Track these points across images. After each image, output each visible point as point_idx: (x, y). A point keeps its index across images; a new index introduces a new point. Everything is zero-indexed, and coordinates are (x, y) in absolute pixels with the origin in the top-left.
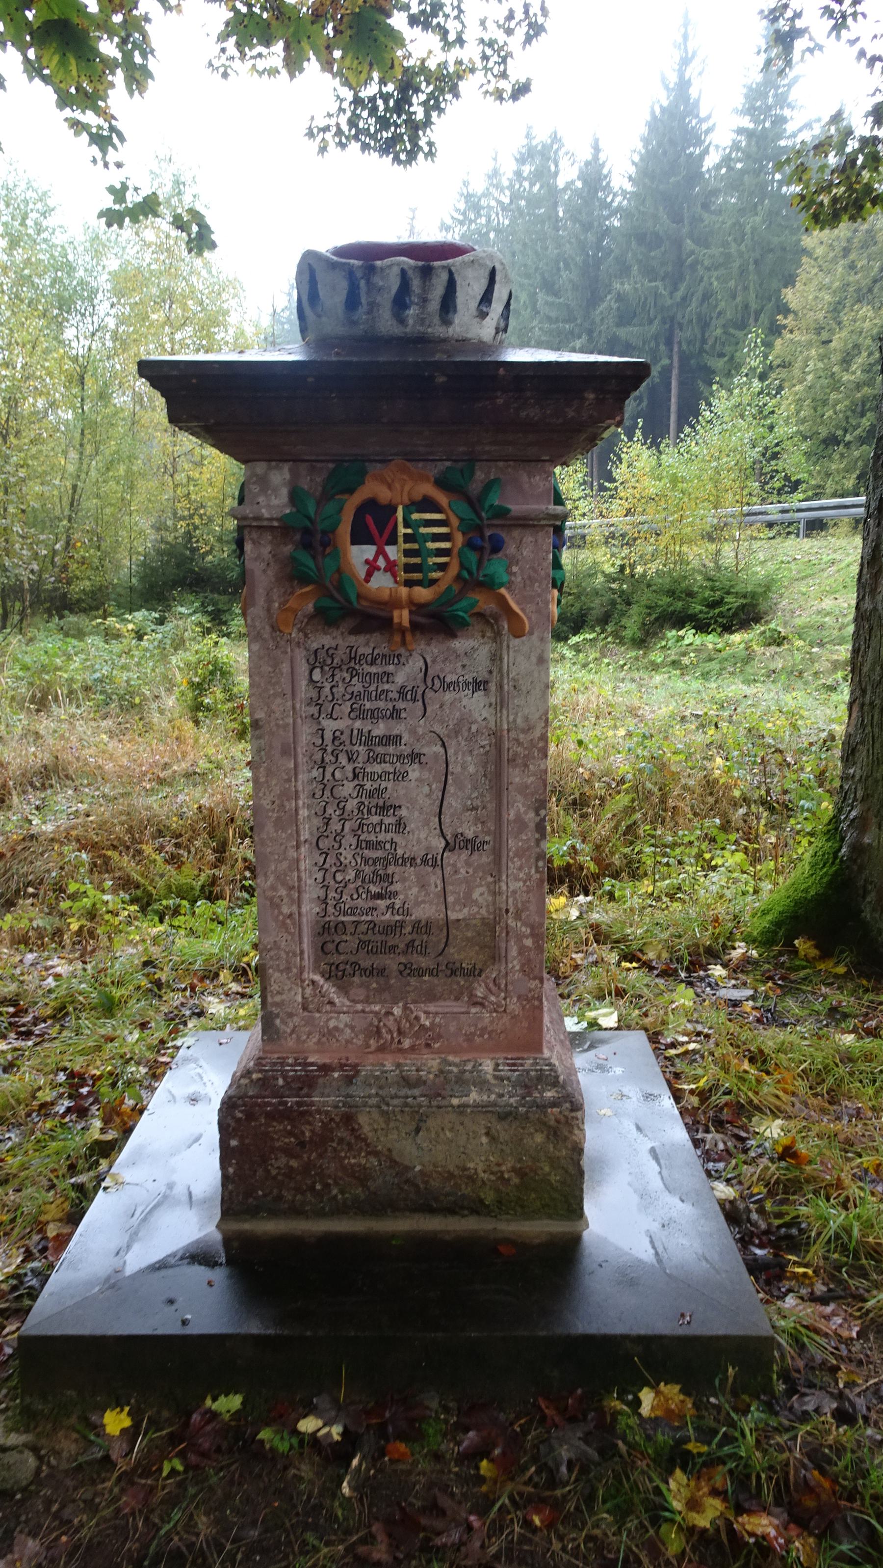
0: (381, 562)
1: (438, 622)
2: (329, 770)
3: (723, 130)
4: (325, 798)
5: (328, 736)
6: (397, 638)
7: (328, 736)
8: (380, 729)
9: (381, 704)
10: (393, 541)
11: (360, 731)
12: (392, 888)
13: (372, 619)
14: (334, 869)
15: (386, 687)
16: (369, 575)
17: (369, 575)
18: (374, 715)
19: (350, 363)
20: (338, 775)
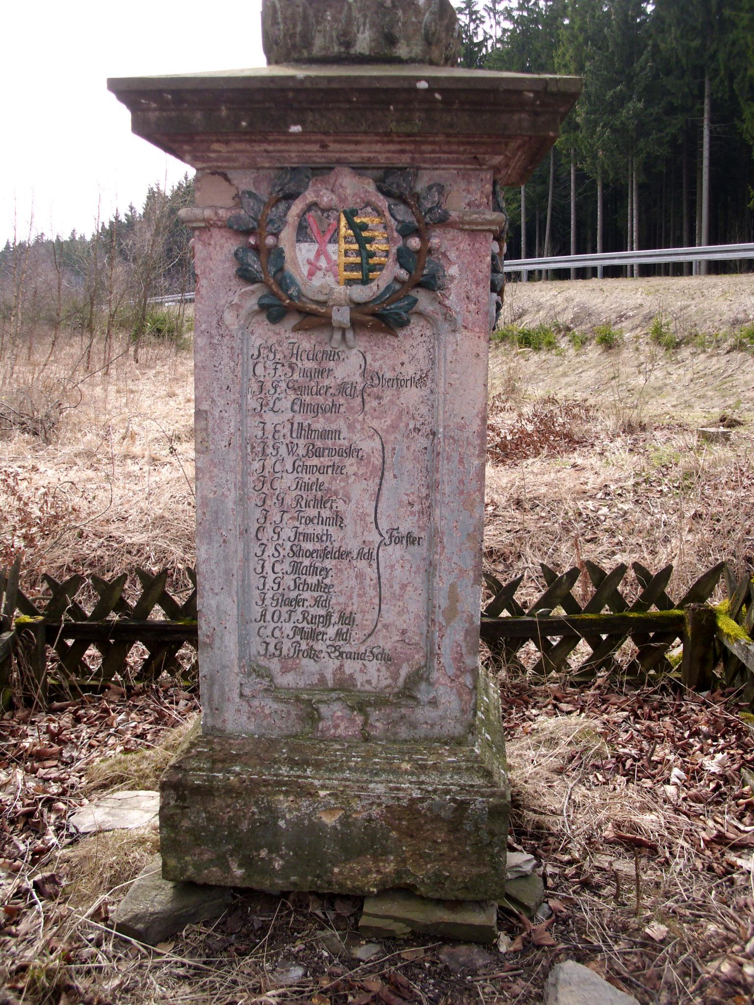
0: (323, 263)
1: (381, 320)
2: (269, 462)
3: (12, 241)
4: (265, 490)
5: (269, 428)
6: (338, 336)
7: (269, 428)
8: (320, 424)
9: (320, 399)
10: (334, 240)
11: (300, 425)
12: (327, 581)
13: (313, 318)
14: (273, 560)
15: (327, 382)
16: (311, 274)
17: (311, 274)
18: (317, 410)
19: (292, 78)
20: (278, 467)
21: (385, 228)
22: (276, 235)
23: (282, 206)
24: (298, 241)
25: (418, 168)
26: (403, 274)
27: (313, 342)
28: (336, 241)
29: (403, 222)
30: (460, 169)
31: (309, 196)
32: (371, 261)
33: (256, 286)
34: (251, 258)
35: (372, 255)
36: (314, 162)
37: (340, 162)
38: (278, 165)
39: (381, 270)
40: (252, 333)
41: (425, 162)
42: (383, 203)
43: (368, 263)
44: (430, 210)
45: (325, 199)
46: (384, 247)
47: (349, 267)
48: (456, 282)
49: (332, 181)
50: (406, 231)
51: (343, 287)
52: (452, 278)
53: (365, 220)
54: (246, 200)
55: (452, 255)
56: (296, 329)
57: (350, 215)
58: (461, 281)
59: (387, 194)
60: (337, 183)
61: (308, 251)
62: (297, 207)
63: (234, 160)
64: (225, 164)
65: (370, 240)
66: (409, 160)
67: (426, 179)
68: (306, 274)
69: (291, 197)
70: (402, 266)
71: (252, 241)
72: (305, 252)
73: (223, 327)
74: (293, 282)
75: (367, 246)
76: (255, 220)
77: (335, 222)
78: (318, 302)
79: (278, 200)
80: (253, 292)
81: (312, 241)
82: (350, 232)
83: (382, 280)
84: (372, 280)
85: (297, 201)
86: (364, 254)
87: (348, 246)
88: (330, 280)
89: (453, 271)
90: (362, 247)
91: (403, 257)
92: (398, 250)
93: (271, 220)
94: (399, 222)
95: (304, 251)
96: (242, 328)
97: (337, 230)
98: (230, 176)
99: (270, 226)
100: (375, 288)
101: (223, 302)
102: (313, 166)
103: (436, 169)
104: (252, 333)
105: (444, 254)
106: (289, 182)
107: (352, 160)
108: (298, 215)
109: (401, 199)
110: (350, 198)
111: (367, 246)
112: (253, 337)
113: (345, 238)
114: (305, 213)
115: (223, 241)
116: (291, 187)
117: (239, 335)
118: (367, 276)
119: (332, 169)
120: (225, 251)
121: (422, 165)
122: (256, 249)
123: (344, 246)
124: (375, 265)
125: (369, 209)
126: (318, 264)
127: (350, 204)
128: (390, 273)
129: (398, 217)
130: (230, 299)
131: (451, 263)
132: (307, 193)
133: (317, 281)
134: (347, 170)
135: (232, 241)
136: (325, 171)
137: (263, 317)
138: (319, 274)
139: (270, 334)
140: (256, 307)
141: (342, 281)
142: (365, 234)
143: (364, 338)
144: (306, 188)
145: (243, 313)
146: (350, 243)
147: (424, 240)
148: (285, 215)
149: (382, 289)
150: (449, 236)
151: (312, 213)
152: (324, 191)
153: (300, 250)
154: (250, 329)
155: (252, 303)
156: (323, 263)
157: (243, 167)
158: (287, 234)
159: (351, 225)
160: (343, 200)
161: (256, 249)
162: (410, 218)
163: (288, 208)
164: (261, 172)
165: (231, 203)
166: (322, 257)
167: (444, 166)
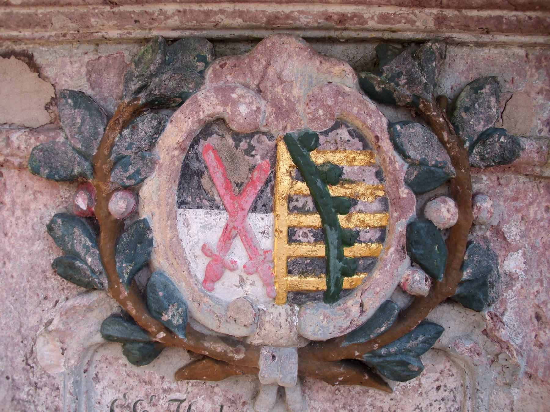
13: (218, 360)
17: (212, 277)
21: (379, 175)
22: (133, 190)
23: (145, 124)
24: (182, 204)
25: (449, 42)
26: (419, 282)
27: (218, 399)
28: (268, 208)
29: (422, 163)
30: (534, 45)
31: (206, 102)
32: (348, 252)
33: (94, 296)
34: (81, 241)
35: (349, 238)
36: (216, 26)
37: (274, 25)
38: (138, 33)
39: (369, 269)
40: (97, 379)
41: (466, 28)
42: (376, 120)
43: (340, 257)
44: (483, 137)
45: (243, 109)
46: (376, 220)
47: (295, 266)
48: (518, 285)
49: (257, 68)
50: (427, 183)
51: (283, 309)
52: (511, 278)
53: (336, 158)
54: (68, 111)
55: (513, 231)
56: (182, 375)
57: (302, 145)
58: (528, 283)
59: (384, 99)
60: (271, 71)
61: (205, 227)
62: (178, 128)
63: (44, 24)
64: (27, 33)
65: (346, 206)
66: (431, 24)
67: (460, 65)
68: (201, 276)
69: (162, 105)
70: (415, 261)
71: (82, 202)
72: (200, 227)
73: (37, 370)
74: (172, 297)
75: (341, 218)
76: (85, 156)
77: (265, 164)
78: (227, 339)
79: (137, 112)
80: (90, 309)
81: (214, 206)
82: (302, 186)
83: (370, 294)
84: (349, 291)
85: (178, 114)
86: (333, 236)
87: (295, 219)
88: (256, 290)
89: (513, 263)
90: (329, 221)
91: (420, 243)
92: (410, 226)
93: (120, 159)
94: (413, 164)
95: (195, 228)
96: (74, 372)
97: (271, 181)
98: (39, 60)
99: (118, 171)
100: (355, 310)
101: (33, 321)
102: (215, 34)
103: (480, 45)
104: (97, 379)
105: (498, 231)
106: (159, 72)
107: (304, 20)
108: (180, 147)
109: (416, 112)
110: (300, 108)
111: (341, 218)
112: (99, 387)
113: (290, 199)
114: (196, 141)
115: (28, 197)
116: (167, 82)
117: (69, 384)
118: (338, 283)
119: (257, 41)
120: (33, 217)
121: (457, 36)
122: (91, 222)
123: (285, 218)
124: (355, 260)
125: (343, 133)
126: (228, 258)
127: (303, 122)
128: (391, 276)
129: (412, 153)
130: (47, 317)
131: (508, 247)
132: (200, 95)
133: (227, 290)
134: (293, 44)
135: (44, 198)
136: (242, 47)
137: (116, 350)
138: (230, 278)
139: (132, 382)
140: (98, 338)
141: (283, 295)
142: (335, 191)
143: (322, 395)
144: (198, 85)
145: (74, 346)
146: (302, 211)
147: (465, 200)
148: (152, 145)
149: (370, 311)
150: (508, 192)
151: (214, 140)
152: (240, 91)
153: (187, 224)
154: (92, 371)
155: (88, 330)
156: (238, 253)
157: (62, 39)
158: (157, 191)
159: (304, 170)
160: (283, 111)
161: (91, 222)
162: (437, 156)
163: (159, 130)
164: (105, 50)
165: (42, 117)
166: (238, 245)
167: (502, 38)
